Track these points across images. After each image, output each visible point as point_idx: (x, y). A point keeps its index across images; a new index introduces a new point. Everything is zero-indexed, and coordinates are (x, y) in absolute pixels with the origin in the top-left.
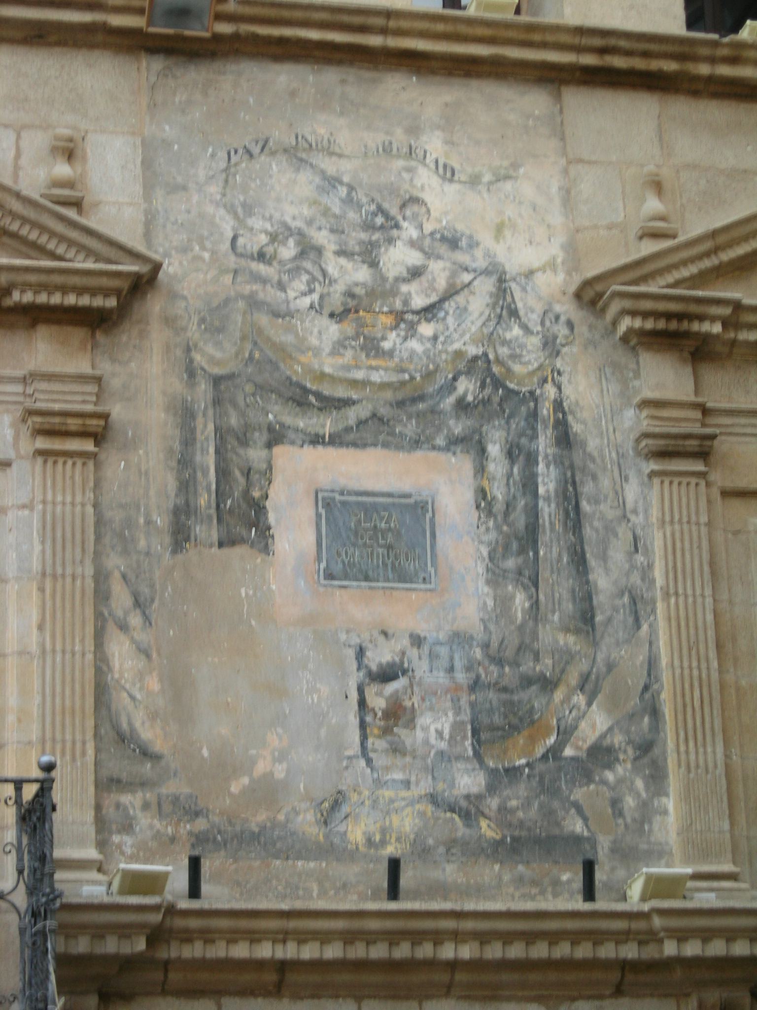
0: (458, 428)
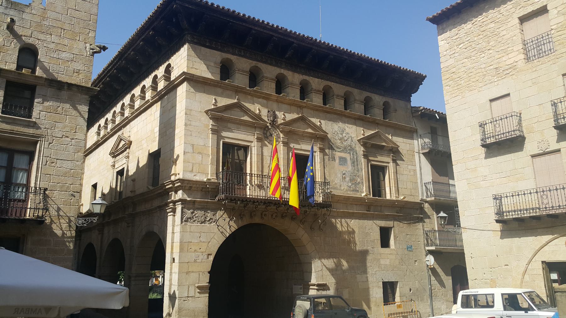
0: (349, 151)
